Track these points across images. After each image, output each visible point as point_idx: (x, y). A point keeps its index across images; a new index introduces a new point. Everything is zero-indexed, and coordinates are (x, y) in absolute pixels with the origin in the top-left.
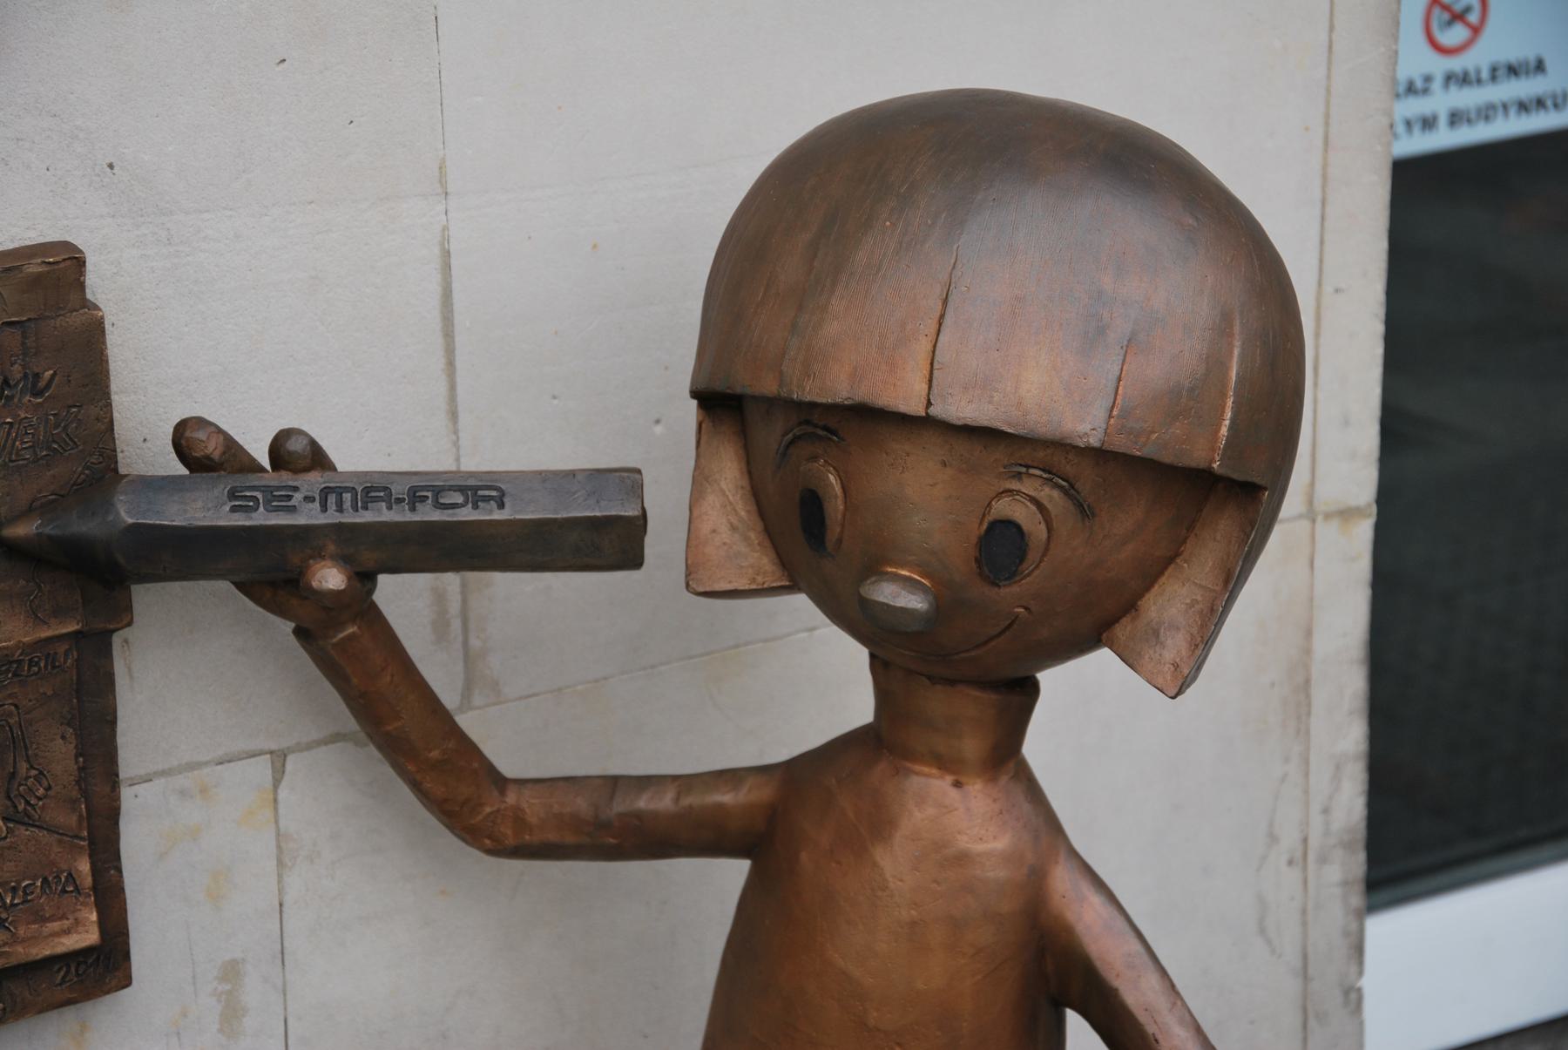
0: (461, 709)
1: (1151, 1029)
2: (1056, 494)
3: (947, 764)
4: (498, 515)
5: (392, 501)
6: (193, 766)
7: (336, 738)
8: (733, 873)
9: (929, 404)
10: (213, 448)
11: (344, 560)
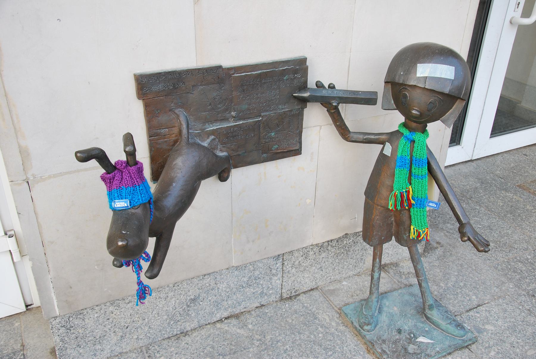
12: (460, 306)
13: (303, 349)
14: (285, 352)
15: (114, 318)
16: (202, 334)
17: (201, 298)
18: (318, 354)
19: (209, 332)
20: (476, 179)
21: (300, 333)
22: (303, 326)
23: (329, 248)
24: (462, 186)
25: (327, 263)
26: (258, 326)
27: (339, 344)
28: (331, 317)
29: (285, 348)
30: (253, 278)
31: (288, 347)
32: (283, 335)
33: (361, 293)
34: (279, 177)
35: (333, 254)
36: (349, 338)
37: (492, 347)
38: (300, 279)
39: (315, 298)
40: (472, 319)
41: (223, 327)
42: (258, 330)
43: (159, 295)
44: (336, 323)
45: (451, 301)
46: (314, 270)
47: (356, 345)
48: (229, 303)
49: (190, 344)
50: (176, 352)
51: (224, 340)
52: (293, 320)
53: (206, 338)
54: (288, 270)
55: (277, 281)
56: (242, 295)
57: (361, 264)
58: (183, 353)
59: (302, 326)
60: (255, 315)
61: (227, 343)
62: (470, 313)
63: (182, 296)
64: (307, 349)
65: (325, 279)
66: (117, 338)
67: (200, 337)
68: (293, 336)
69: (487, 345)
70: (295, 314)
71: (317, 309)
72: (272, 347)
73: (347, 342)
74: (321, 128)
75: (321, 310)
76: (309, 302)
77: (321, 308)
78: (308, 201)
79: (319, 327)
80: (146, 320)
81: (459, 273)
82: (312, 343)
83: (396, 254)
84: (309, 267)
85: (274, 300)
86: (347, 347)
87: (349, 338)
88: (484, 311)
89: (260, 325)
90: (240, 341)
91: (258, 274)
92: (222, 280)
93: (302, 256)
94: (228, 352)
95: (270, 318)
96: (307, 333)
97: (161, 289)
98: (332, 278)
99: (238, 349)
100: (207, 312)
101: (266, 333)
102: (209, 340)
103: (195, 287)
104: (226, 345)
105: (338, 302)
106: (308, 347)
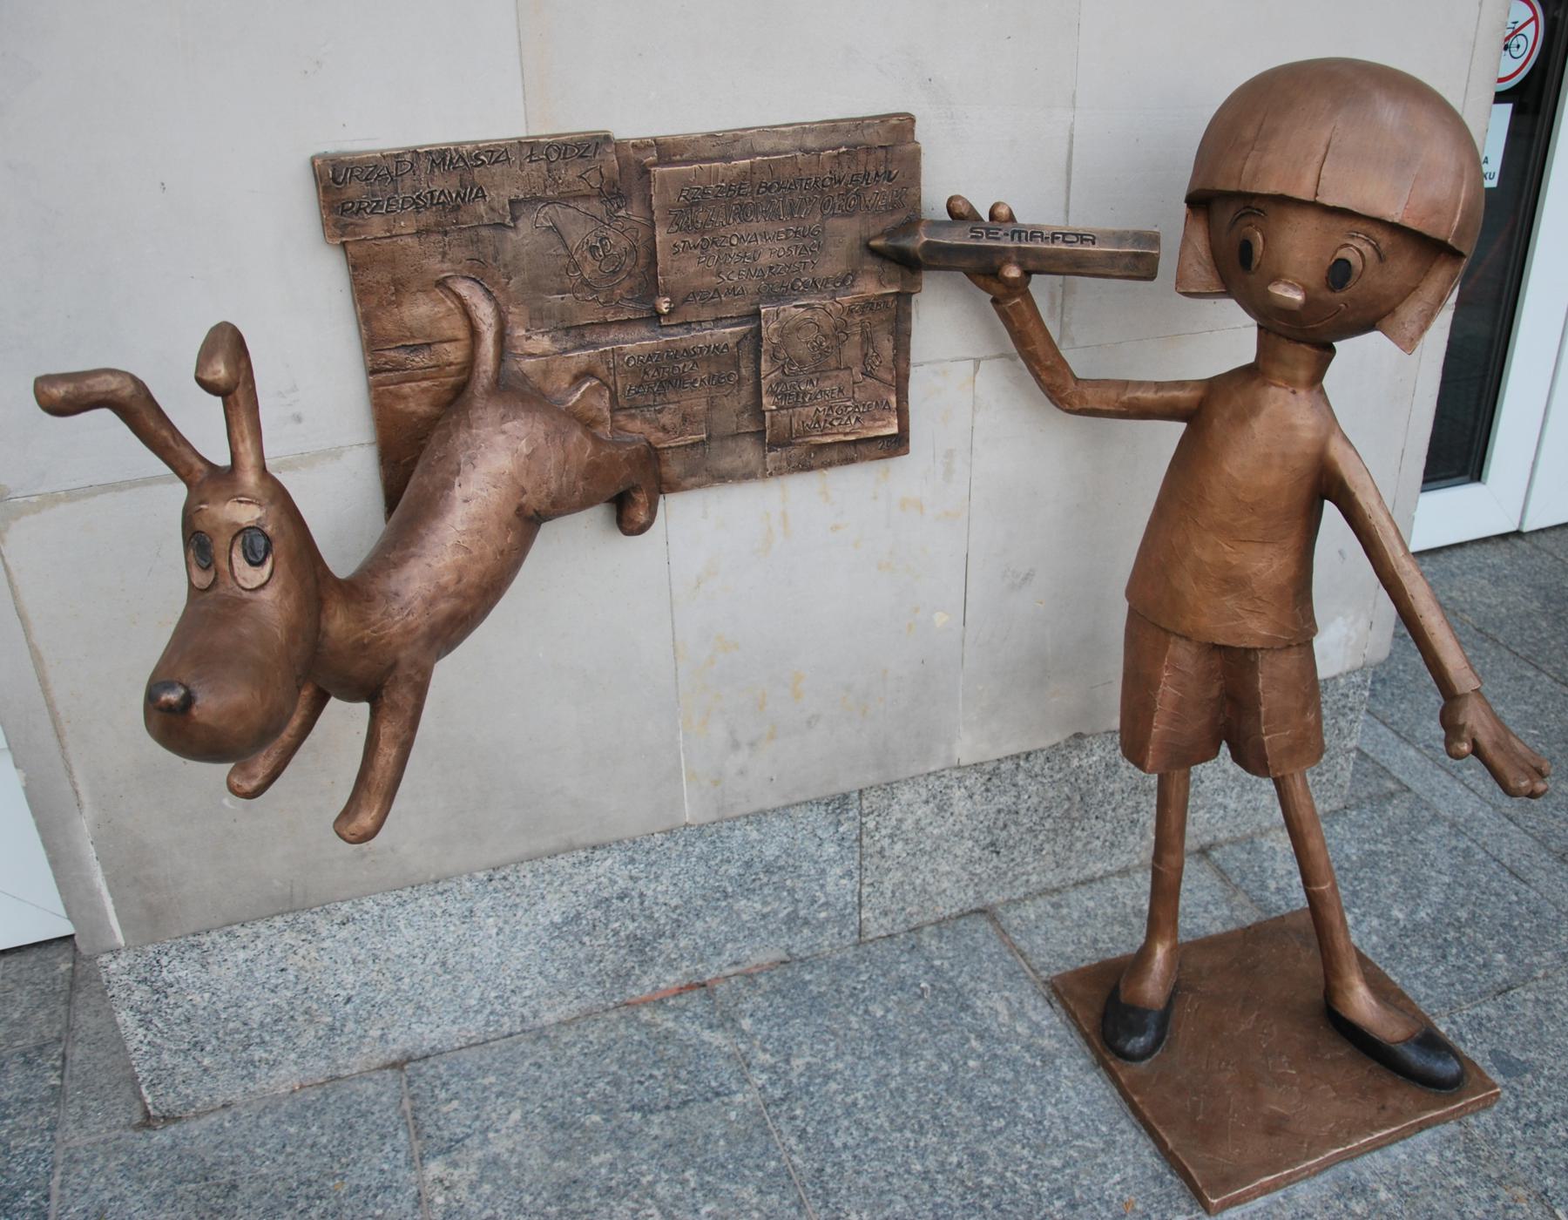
1: (1368, 512)
2: (1369, 247)
3: (1291, 382)
4: (1091, 248)
7: (1001, 356)
8: (1179, 428)
9: (1316, 195)
10: (964, 210)
11: (1020, 265)
12: (1453, 985)
13: (910, 1107)
14: (848, 1114)
15: (302, 968)
16: (591, 1038)
17: (584, 922)
18: (957, 1124)
19: (613, 1035)
20: (1529, 586)
21: (904, 1053)
22: (920, 1032)
23: (1021, 778)
24: (1484, 609)
25: (1013, 829)
26: (771, 1023)
27: (1031, 1094)
28: (1017, 1005)
29: (849, 1100)
30: (758, 866)
31: (859, 1095)
32: (849, 1058)
33: (1126, 932)
34: (835, 528)
35: (1035, 800)
36: (1066, 1077)
37: (1549, 1122)
38: (921, 876)
39: (970, 943)
40: (1488, 1030)
41: (659, 1021)
42: (769, 1037)
43: (443, 904)
44: (1029, 1028)
45: (1423, 969)
46: (971, 850)
47: (1087, 1103)
48: (681, 945)
49: (546, 1066)
50: (500, 1088)
51: (655, 1063)
52: (888, 1010)
53: (600, 1053)
54: (879, 845)
55: (843, 882)
56: (725, 922)
57: (1131, 838)
58: (521, 1093)
59: (917, 1030)
60: (768, 989)
61: (663, 1070)
62: (1485, 1008)
63: (520, 913)
64: (922, 1107)
65: (1010, 883)
66: (317, 1032)
67: (582, 1048)
68: (882, 1062)
69: (1532, 1117)
70: (899, 992)
71: (972, 978)
72: (807, 1093)
73: (1058, 1089)
74: (976, 369)
75: (982, 981)
76: (951, 954)
77: (986, 976)
78: (940, 619)
79: (973, 1036)
80: (407, 980)
81: (1455, 876)
82: (941, 1086)
83: (1251, 812)
84: (953, 838)
85: (834, 941)
86: (1056, 1105)
87: (1066, 1077)
88: (1530, 1004)
89: (779, 1021)
90: (708, 1070)
91: (777, 853)
92: (654, 869)
93: (927, 802)
94: (663, 1100)
95: (814, 998)
96: (929, 1054)
97: (448, 886)
98: (1034, 878)
99: (696, 1094)
100: (610, 967)
101: (795, 1048)
102: (608, 1061)
103: (562, 884)
104: (660, 1078)
105: (1046, 959)
106: (927, 1099)
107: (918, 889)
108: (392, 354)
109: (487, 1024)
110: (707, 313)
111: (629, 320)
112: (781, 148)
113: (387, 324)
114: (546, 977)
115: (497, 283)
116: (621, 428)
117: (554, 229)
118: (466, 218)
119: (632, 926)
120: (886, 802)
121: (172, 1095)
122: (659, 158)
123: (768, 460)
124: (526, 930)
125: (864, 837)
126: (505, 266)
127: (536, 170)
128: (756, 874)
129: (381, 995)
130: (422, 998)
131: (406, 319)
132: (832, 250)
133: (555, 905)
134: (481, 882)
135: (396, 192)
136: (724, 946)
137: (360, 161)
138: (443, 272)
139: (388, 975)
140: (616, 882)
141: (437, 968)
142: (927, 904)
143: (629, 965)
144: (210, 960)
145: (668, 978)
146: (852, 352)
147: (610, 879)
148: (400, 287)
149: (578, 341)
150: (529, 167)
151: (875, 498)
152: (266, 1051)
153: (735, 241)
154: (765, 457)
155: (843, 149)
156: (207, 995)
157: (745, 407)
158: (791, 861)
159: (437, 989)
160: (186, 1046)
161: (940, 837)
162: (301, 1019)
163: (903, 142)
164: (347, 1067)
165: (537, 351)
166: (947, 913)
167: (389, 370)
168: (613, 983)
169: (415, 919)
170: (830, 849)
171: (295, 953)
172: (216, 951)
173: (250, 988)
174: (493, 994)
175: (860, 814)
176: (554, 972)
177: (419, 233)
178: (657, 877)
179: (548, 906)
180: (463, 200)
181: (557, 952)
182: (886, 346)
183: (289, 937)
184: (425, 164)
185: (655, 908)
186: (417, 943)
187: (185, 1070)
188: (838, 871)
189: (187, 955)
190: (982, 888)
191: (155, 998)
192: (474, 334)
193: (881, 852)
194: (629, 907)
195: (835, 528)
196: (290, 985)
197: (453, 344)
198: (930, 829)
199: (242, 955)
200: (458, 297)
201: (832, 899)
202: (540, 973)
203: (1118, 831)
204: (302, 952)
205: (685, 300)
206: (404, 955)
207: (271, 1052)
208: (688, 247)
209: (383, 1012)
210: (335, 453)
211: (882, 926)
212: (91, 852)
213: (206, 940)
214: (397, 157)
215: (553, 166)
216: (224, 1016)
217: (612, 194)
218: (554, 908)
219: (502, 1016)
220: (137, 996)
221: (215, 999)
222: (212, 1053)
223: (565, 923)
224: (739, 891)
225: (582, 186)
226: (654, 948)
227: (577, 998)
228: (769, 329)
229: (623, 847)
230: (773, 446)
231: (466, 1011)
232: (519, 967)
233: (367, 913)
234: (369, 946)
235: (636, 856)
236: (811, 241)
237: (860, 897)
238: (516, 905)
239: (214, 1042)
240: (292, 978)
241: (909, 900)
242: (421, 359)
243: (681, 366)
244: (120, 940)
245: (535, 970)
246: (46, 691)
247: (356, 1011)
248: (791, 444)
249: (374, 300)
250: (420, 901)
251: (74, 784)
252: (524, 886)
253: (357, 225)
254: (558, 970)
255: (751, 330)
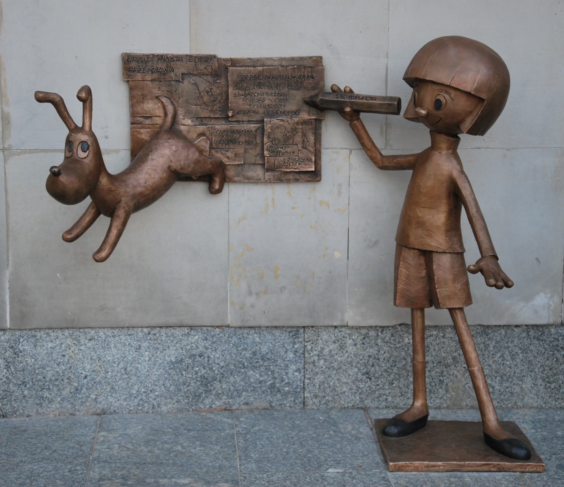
0: (383, 149)
5: (359, 98)
6: (336, 148)
15: (71, 357)
30: (258, 356)
34: (293, 208)
35: (387, 355)
43: (129, 340)
55: (296, 374)
57: (440, 390)
63: (159, 353)
65: (378, 398)
80: (110, 373)
91: (267, 351)
92: (215, 345)
100: (192, 390)
103: (177, 343)
107: (332, 388)
108: (139, 118)
109: (138, 405)
110: (245, 118)
111: (218, 117)
112: (274, 64)
113: (139, 109)
114: (165, 387)
115: (175, 100)
116: (213, 155)
117: (195, 84)
118: (167, 77)
119: (203, 371)
120: (316, 337)
121: (9, 405)
122: (231, 64)
123: (266, 175)
124: (160, 361)
125: (306, 352)
126: (179, 94)
127: (191, 65)
128: (258, 359)
129: (99, 378)
130: (114, 384)
131: (145, 108)
132: (291, 101)
133: (173, 352)
134: (145, 334)
135: (146, 67)
136: (242, 393)
137: (136, 56)
138: (158, 94)
139: (103, 369)
140: (199, 348)
141: (123, 370)
142: (336, 397)
143: (200, 391)
144: (38, 344)
145: (216, 403)
146: (298, 138)
147: (196, 346)
148: (144, 97)
149: (200, 123)
150: (188, 63)
151: (309, 198)
152: (49, 394)
153: (256, 95)
154: (265, 174)
155: (296, 66)
156: (33, 360)
157: (258, 154)
158: (273, 357)
159: (121, 382)
160: (20, 383)
161: (341, 362)
162: (66, 381)
163: (318, 65)
164: (79, 411)
165: (186, 124)
166: (346, 405)
167: (137, 124)
168: (193, 399)
169: (118, 345)
170: (291, 355)
171: (70, 349)
172: (41, 341)
173: (50, 361)
174: (143, 390)
175: (304, 340)
176: (169, 385)
177: (152, 80)
178: (216, 350)
179: (170, 352)
180: (167, 71)
181: (171, 376)
182: (311, 138)
183: (69, 341)
184: (156, 59)
185: (214, 365)
186: (116, 356)
187: (16, 394)
188: (294, 367)
189: (30, 340)
190: (363, 396)
191: (14, 356)
192: (166, 114)
193: (314, 362)
194: (203, 361)
195: (293, 208)
196: (65, 363)
197: (159, 118)
198: (336, 357)
199: (50, 345)
200: (162, 102)
201: (291, 382)
202: (163, 385)
203: (433, 384)
204: (72, 349)
205: (238, 113)
206: (111, 361)
207: (51, 394)
208: (240, 95)
209: (98, 386)
210: (117, 151)
211: (314, 403)
212: (7, 285)
213: (38, 334)
214: (148, 56)
215: (197, 63)
216: (37, 372)
217: (216, 75)
218: (172, 354)
219: (145, 402)
220: (7, 354)
221: (36, 363)
222: (28, 389)
223: (176, 363)
224: (250, 365)
225: (206, 71)
226: (211, 385)
227: (177, 402)
228: (267, 127)
229: (203, 332)
230: (268, 170)
231: (131, 396)
232: (155, 379)
233: (100, 337)
234: (98, 353)
235: (208, 337)
236: (284, 98)
237: (304, 385)
238: (158, 348)
239: (31, 383)
240: (66, 360)
241: (327, 393)
242: (148, 122)
243: (235, 136)
244: (8, 325)
245: (161, 382)
246: (7, 219)
247: (88, 383)
248: (274, 170)
249: (135, 100)
250: (121, 337)
251: (8, 256)
252: (162, 340)
253: (133, 75)
254: (171, 385)
255: (260, 126)
